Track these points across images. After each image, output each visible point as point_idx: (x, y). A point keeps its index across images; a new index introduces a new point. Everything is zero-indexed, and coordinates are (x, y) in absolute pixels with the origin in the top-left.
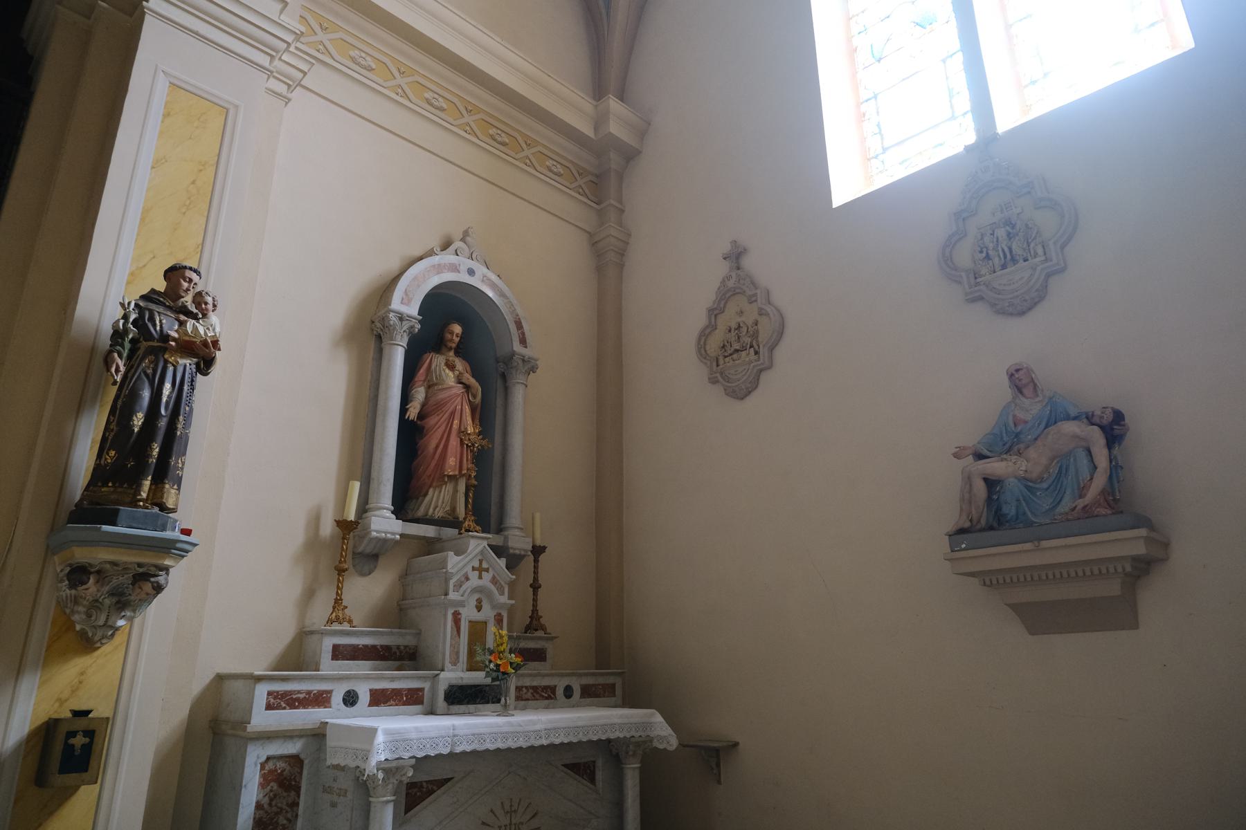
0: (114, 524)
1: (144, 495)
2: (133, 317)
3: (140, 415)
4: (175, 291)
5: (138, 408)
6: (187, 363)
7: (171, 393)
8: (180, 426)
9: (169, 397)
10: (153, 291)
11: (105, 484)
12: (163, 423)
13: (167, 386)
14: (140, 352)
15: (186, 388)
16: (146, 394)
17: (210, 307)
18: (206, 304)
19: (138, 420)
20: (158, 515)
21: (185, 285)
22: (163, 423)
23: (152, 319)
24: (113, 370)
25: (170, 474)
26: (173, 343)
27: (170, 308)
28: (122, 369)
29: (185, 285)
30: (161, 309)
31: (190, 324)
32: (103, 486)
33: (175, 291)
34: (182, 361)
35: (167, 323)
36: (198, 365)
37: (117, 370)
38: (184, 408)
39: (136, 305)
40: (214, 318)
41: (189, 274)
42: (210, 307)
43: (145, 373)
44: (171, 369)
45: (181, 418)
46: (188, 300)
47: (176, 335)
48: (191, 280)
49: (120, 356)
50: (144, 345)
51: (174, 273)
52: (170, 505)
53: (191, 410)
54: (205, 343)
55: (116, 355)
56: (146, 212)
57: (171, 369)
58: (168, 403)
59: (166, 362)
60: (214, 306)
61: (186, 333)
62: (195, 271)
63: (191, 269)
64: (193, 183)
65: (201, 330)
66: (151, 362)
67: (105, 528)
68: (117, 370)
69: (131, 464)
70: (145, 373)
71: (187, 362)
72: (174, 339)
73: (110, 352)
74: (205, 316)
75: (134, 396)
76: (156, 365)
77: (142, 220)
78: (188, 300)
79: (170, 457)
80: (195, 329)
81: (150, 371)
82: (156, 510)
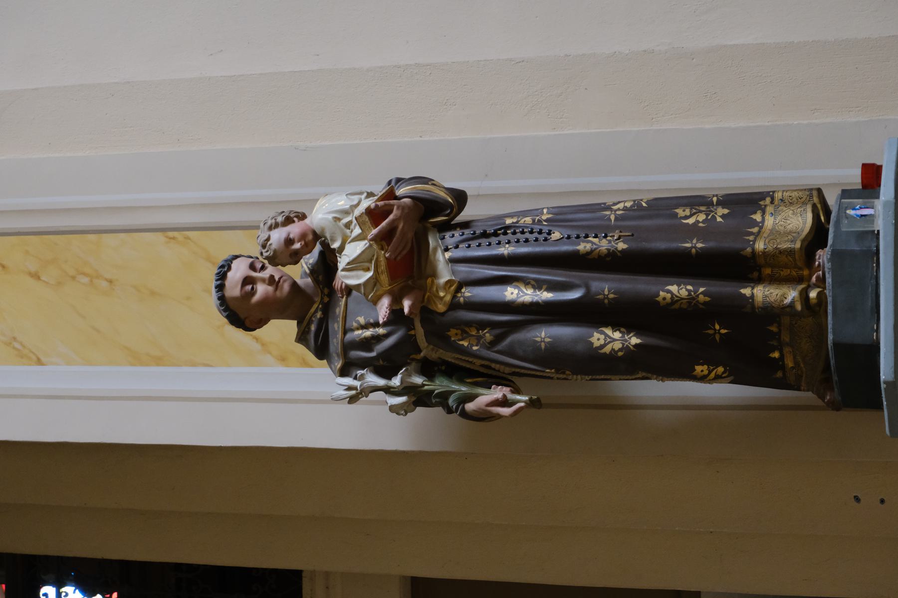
0: (874, 348)
1: (791, 294)
2: (374, 380)
3: (597, 338)
4: (290, 294)
5: (580, 347)
6: (444, 259)
7: (526, 282)
8: (603, 245)
9: (538, 285)
10: (302, 338)
11: (779, 364)
12: (606, 287)
13: (511, 293)
14: (450, 357)
15: (506, 250)
16: (544, 334)
17: (295, 229)
18: (289, 241)
19: (610, 339)
20: (837, 256)
21: (262, 290)
22: (606, 287)
23: (367, 344)
24: (505, 411)
25: (728, 244)
26: (407, 304)
27: (327, 309)
28: (497, 393)
29: (262, 290)
30: (336, 327)
31: (345, 278)
32: (783, 368)
33: (290, 294)
34: (445, 275)
35: (369, 316)
36: (445, 227)
37: (504, 402)
38: (557, 241)
39: (343, 373)
40: (320, 216)
41: (233, 288)
42: (295, 229)
43: (498, 339)
44: (468, 293)
45: (583, 247)
46: (299, 272)
47: (385, 304)
48: (248, 281)
49: (471, 398)
50: (427, 351)
51: (242, 314)
52: (801, 221)
53: (560, 217)
54: (383, 239)
55: (470, 406)
56: (137, 358)
57: (468, 293)
58: (553, 287)
59: (454, 306)
60: (288, 221)
61: (373, 282)
62: (222, 276)
63: (220, 288)
64: (36, 276)
65: (353, 250)
66: (465, 335)
67: (886, 372)
68: (504, 402)
69: (719, 329)
70: (493, 344)
71: (441, 258)
72: (396, 300)
73: (464, 414)
74: (315, 237)
75: (558, 361)
76: (470, 324)
77: (159, 361)
78: (299, 272)
79: (686, 253)
80: (355, 265)
81: (488, 337)
82: (823, 256)
